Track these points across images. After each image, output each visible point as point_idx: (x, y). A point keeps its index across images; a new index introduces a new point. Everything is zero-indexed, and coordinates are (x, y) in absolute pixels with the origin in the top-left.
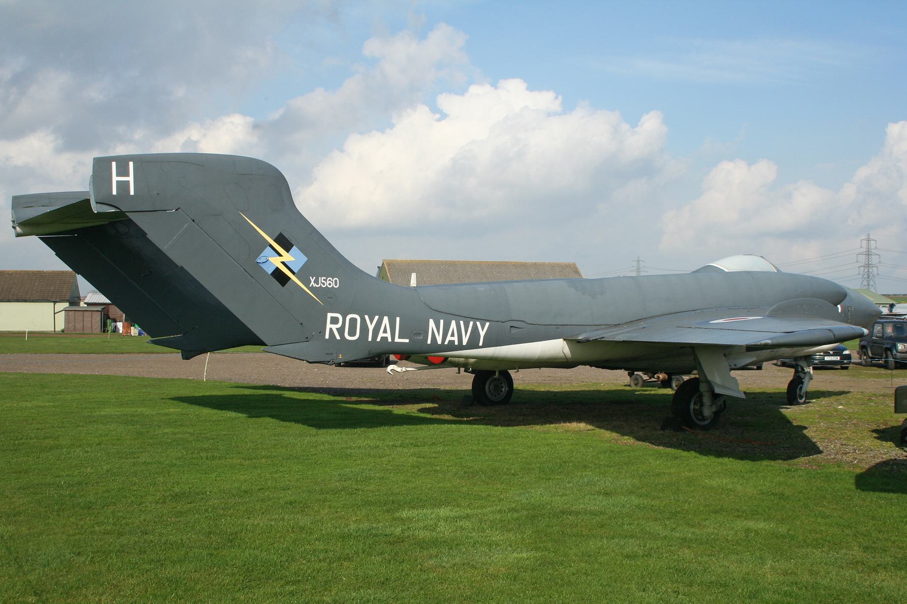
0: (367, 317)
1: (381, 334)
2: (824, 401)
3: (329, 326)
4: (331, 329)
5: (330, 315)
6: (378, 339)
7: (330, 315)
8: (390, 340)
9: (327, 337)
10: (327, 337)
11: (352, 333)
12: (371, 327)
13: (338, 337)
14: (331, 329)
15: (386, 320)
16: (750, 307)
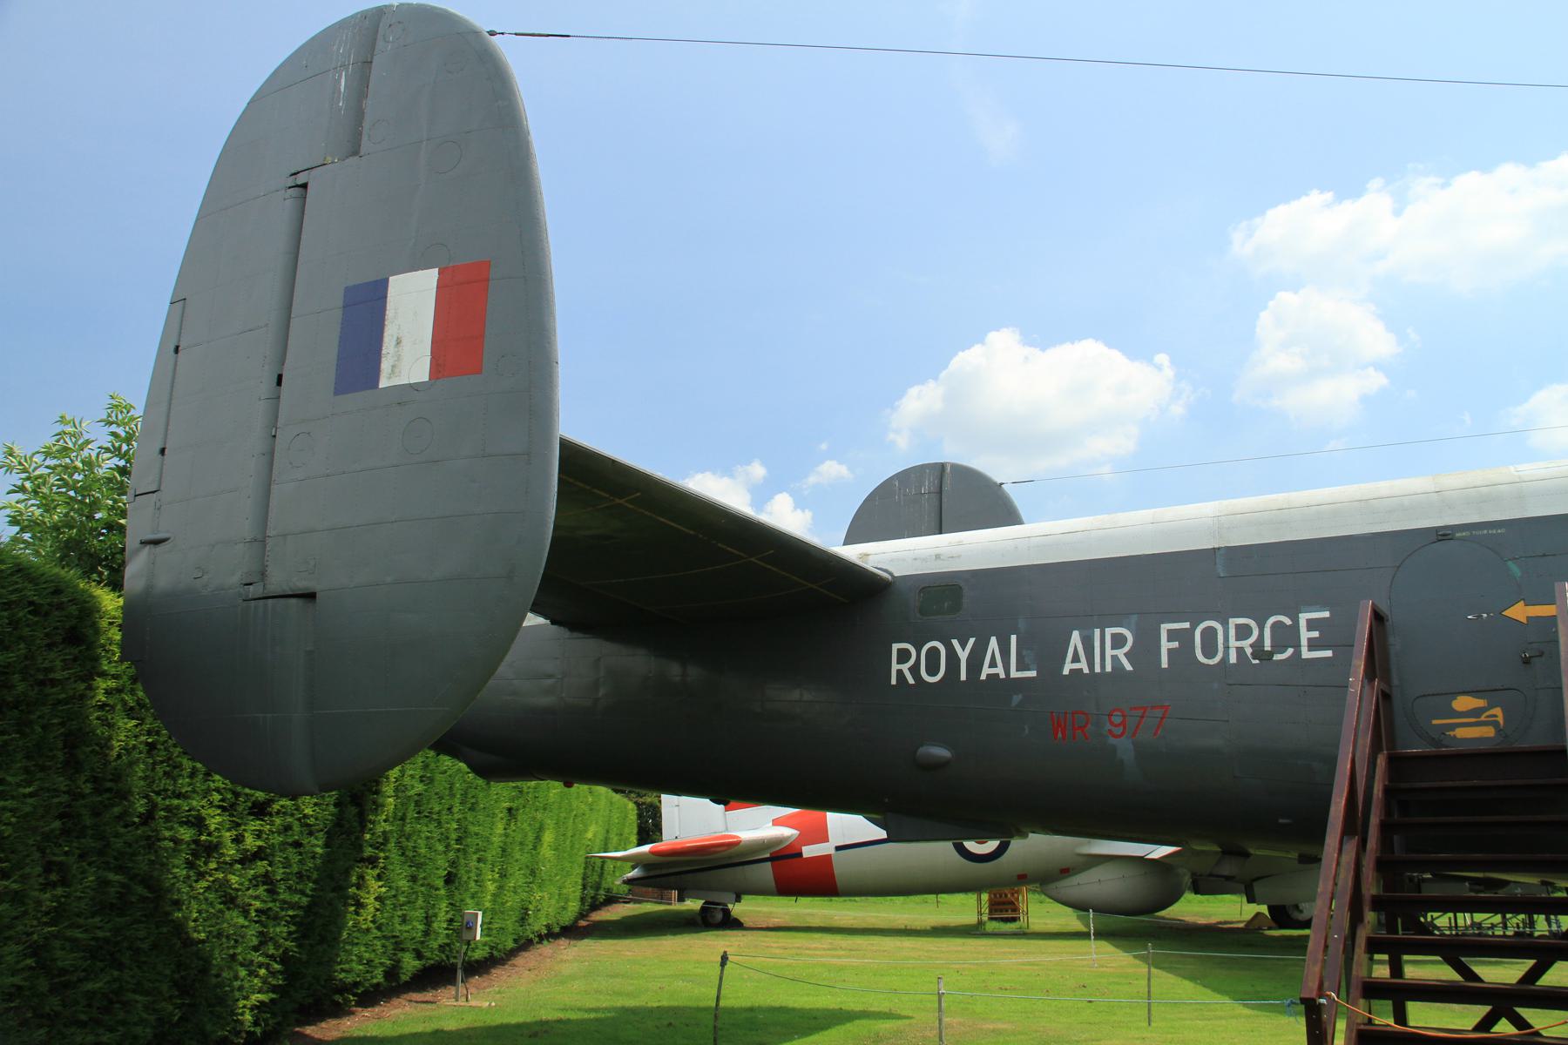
0: (955, 642)
1: (986, 671)
2: (864, 1022)
3: (895, 667)
4: (900, 672)
5: (895, 647)
6: (983, 677)
7: (895, 647)
8: (1086, 671)
9: (894, 682)
10: (894, 682)
11: (932, 670)
12: (963, 655)
13: (911, 681)
14: (900, 672)
15: (993, 642)
16: (1375, 759)
